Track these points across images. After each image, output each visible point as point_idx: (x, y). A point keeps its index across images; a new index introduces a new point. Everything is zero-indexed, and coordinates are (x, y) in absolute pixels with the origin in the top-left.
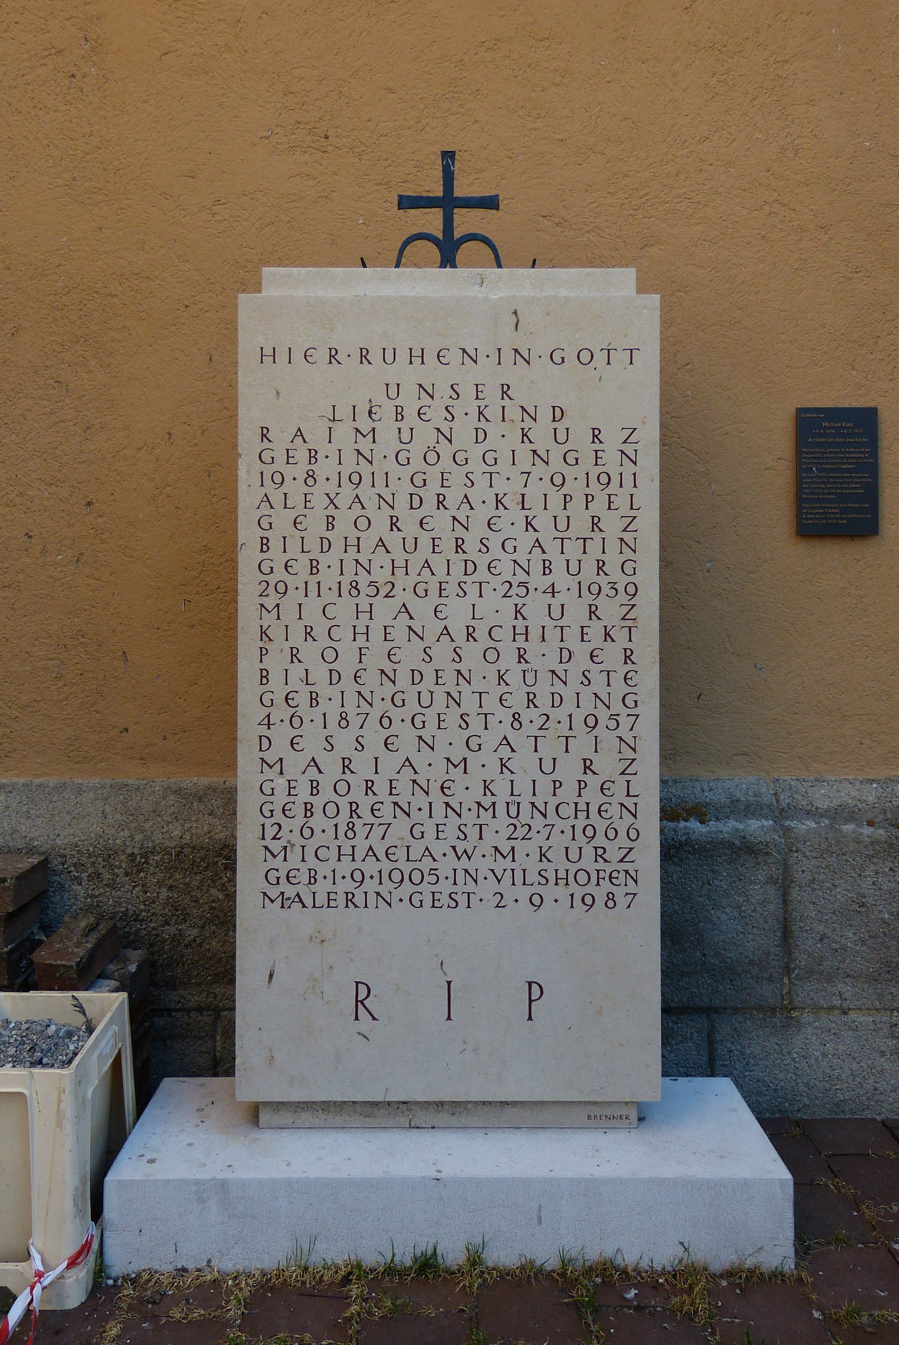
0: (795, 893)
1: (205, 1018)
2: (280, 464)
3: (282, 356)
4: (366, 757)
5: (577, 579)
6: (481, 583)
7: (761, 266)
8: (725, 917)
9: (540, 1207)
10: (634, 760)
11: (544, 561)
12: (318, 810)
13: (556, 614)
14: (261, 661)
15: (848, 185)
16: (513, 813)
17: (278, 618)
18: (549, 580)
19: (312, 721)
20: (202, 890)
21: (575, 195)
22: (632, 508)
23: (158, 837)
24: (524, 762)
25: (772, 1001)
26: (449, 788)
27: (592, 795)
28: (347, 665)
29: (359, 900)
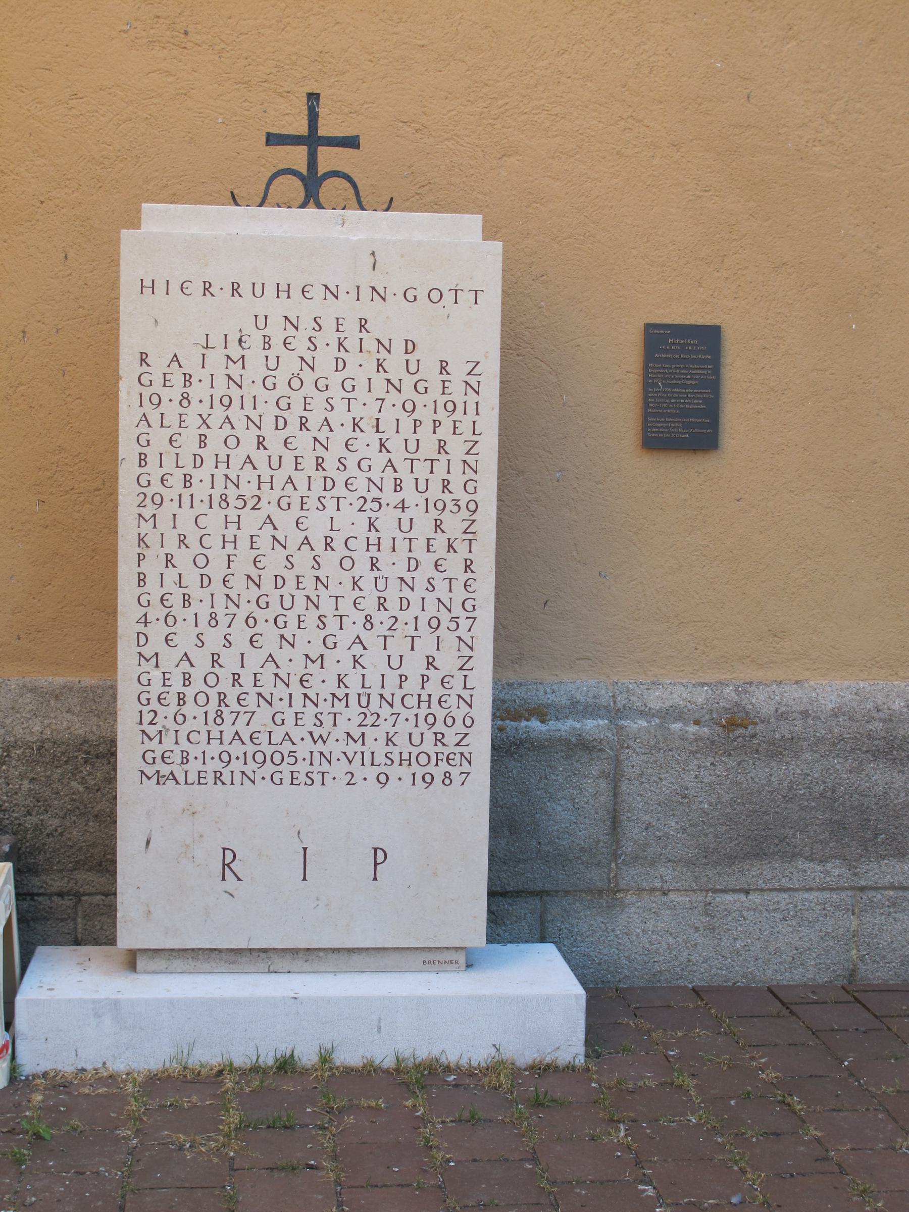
0: (624, 786)
1: (67, 902)
2: (157, 387)
3: (160, 287)
4: (235, 651)
5: (425, 496)
6: (338, 498)
7: (616, 181)
8: (559, 808)
9: (380, 1020)
10: (471, 657)
11: (396, 479)
12: (189, 699)
13: (405, 526)
14: (139, 566)
15: (700, 104)
16: (364, 703)
17: (155, 527)
18: (399, 496)
19: (185, 620)
20: (62, 783)
21: (435, 102)
22: (474, 434)
23: (19, 731)
24: (374, 659)
25: (599, 884)
26: (307, 681)
27: (434, 688)
28: (217, 570)
29: (226, 777)
